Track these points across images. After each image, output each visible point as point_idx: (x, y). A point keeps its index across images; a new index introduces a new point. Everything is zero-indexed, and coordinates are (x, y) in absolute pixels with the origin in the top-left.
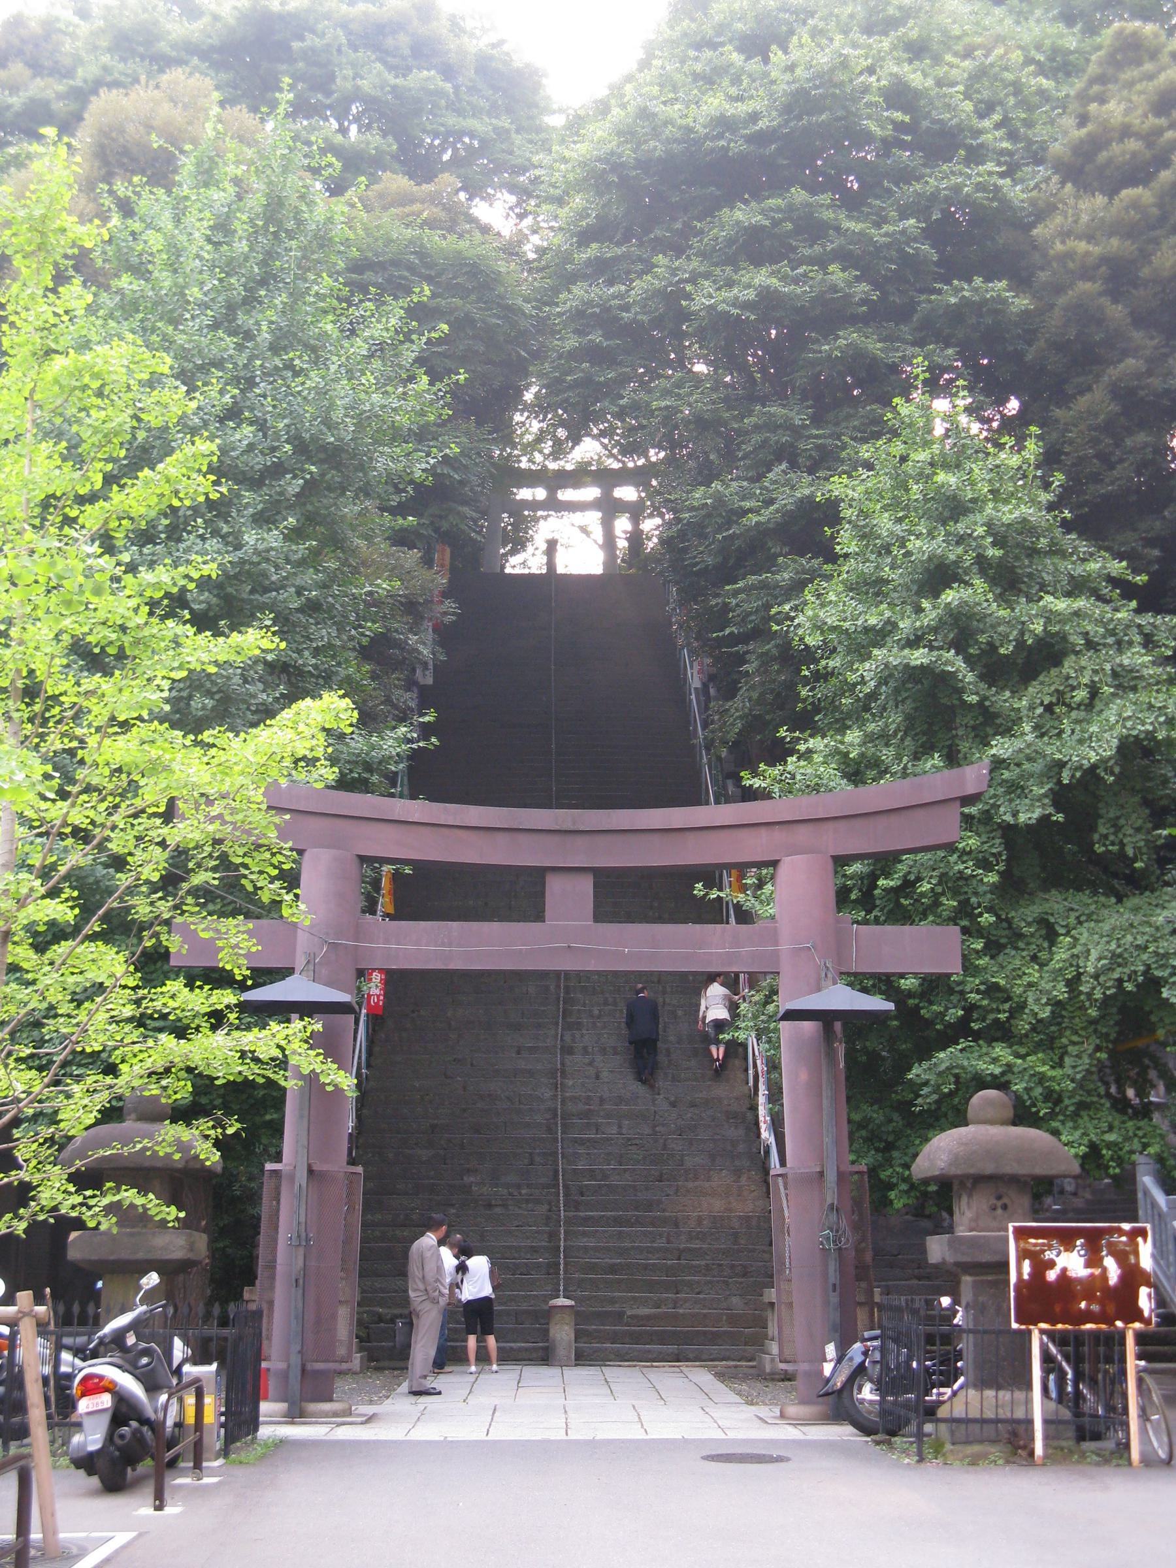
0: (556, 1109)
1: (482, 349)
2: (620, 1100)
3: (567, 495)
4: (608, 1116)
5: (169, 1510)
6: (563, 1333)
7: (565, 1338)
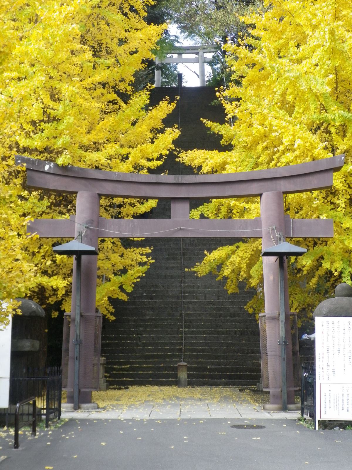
3: (185, 56)
5: (20, 449)
6: (183, 375)
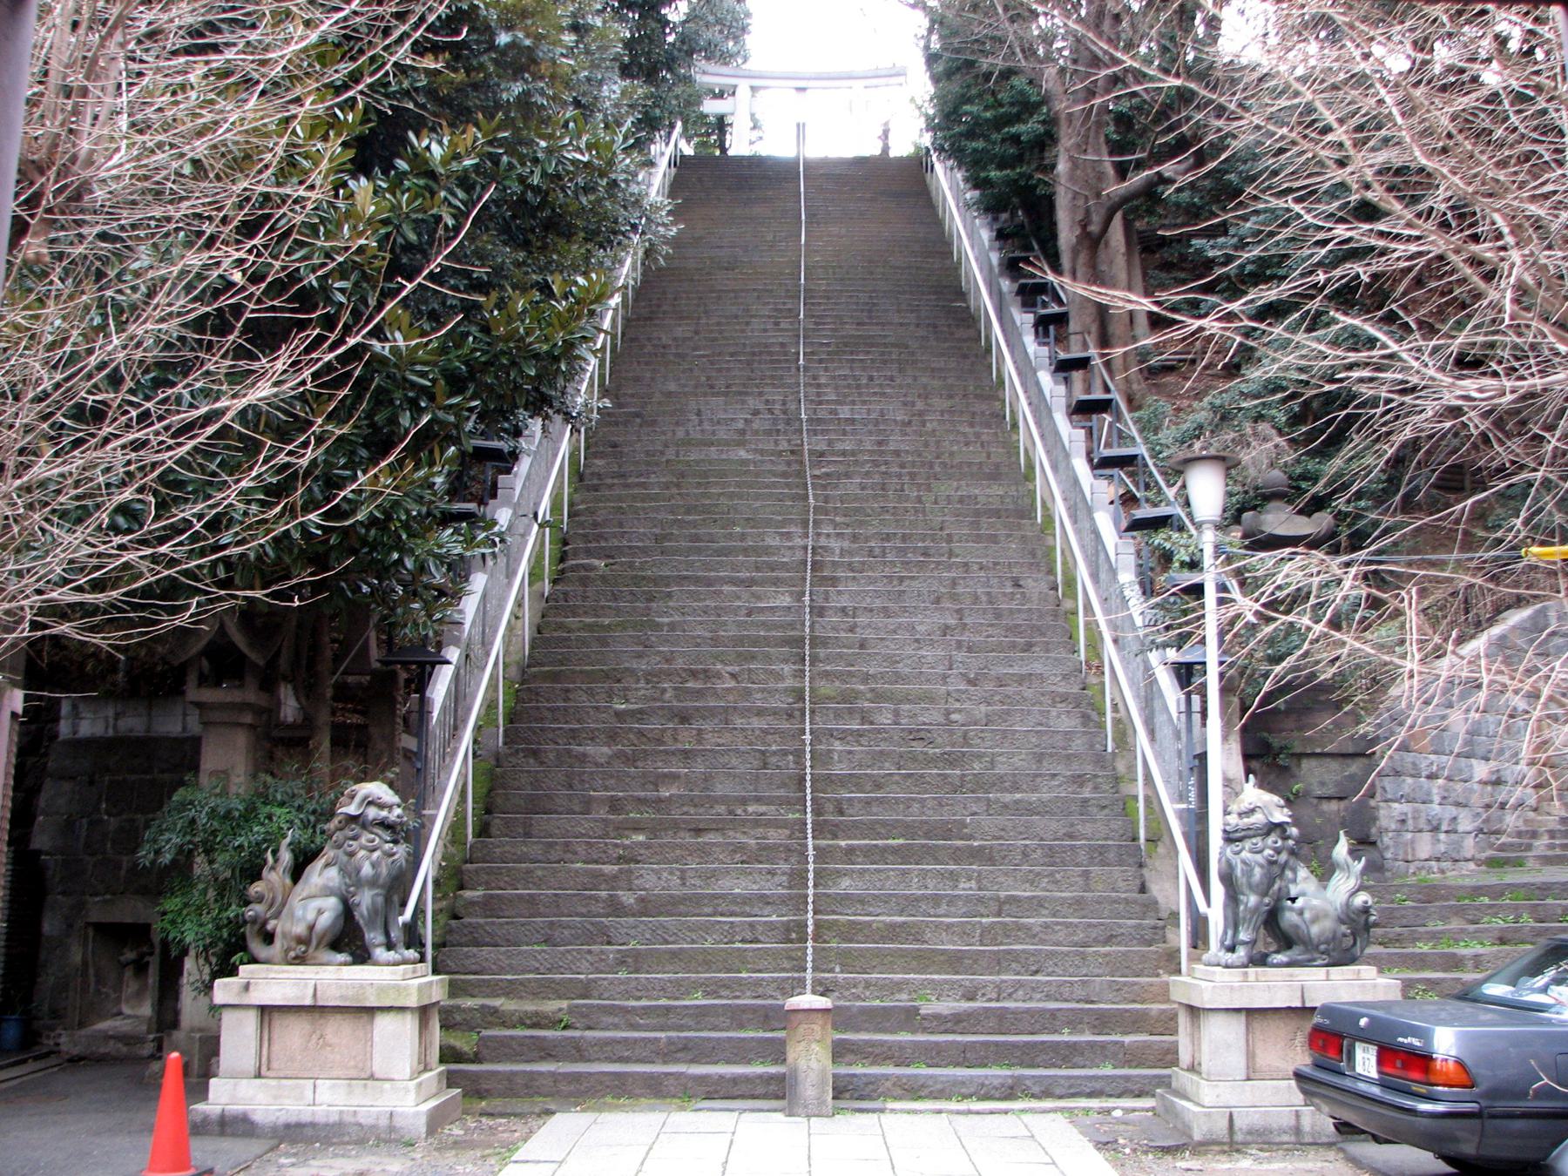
0: (802, 690)
6: (811, 1059)
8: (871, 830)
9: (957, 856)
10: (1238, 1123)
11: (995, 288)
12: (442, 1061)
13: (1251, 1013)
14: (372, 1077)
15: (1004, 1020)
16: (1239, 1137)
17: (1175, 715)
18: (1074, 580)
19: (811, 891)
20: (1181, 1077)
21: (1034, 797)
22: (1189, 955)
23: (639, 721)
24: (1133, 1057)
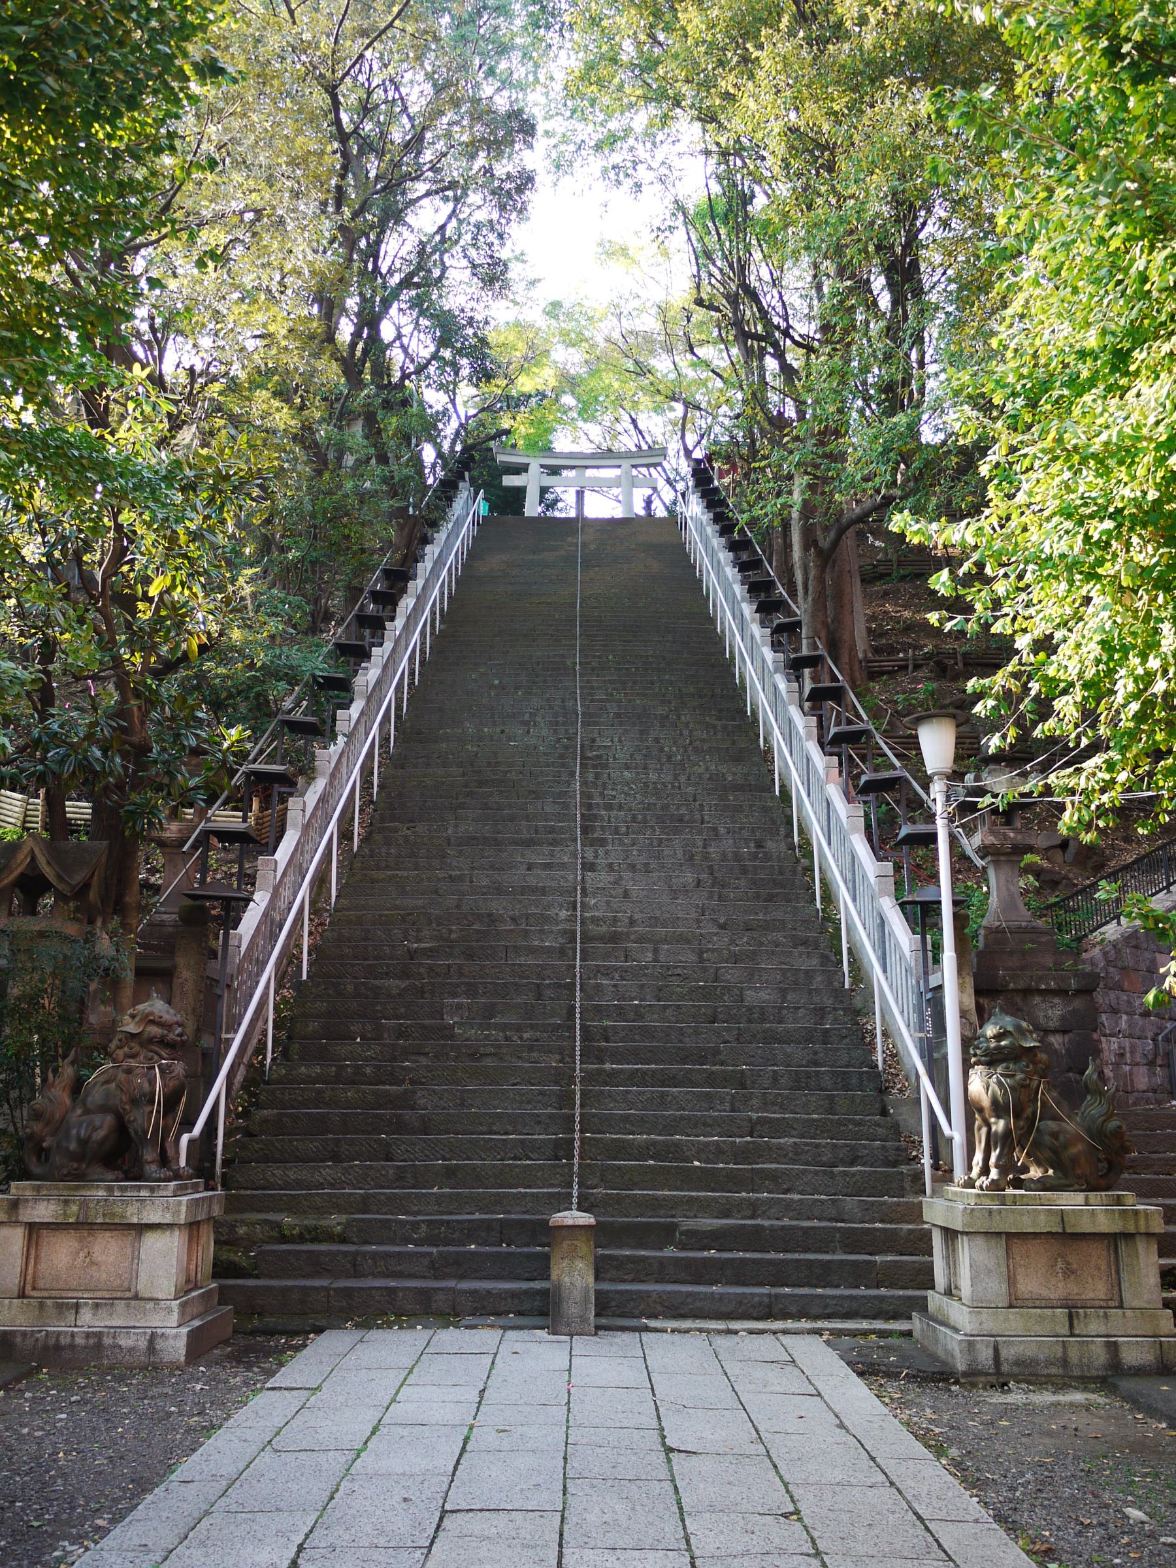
0: (574, 932)
1: (1125, 1017)
2: (654, 921)
4: (641, 940)
6: (575, 1276)
7: (579, 1283)
8: (634, 1055)
9: (711, 1080)
10: (1004, 1353)
11: (738, 613)
12: (215, 1275)
13: (1009, 1236)
14: (136, 1297)
15: (754, 1239)
16: (1005, 1368)
17: (907, 953)
18: (810, 844)
19: (578, 1111)
20: (934, 1299)
21: (781, 1028)
22: (933, 1176)
23: (429, 957)
24: (889, 1276)
